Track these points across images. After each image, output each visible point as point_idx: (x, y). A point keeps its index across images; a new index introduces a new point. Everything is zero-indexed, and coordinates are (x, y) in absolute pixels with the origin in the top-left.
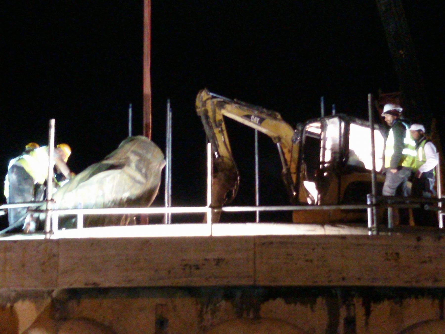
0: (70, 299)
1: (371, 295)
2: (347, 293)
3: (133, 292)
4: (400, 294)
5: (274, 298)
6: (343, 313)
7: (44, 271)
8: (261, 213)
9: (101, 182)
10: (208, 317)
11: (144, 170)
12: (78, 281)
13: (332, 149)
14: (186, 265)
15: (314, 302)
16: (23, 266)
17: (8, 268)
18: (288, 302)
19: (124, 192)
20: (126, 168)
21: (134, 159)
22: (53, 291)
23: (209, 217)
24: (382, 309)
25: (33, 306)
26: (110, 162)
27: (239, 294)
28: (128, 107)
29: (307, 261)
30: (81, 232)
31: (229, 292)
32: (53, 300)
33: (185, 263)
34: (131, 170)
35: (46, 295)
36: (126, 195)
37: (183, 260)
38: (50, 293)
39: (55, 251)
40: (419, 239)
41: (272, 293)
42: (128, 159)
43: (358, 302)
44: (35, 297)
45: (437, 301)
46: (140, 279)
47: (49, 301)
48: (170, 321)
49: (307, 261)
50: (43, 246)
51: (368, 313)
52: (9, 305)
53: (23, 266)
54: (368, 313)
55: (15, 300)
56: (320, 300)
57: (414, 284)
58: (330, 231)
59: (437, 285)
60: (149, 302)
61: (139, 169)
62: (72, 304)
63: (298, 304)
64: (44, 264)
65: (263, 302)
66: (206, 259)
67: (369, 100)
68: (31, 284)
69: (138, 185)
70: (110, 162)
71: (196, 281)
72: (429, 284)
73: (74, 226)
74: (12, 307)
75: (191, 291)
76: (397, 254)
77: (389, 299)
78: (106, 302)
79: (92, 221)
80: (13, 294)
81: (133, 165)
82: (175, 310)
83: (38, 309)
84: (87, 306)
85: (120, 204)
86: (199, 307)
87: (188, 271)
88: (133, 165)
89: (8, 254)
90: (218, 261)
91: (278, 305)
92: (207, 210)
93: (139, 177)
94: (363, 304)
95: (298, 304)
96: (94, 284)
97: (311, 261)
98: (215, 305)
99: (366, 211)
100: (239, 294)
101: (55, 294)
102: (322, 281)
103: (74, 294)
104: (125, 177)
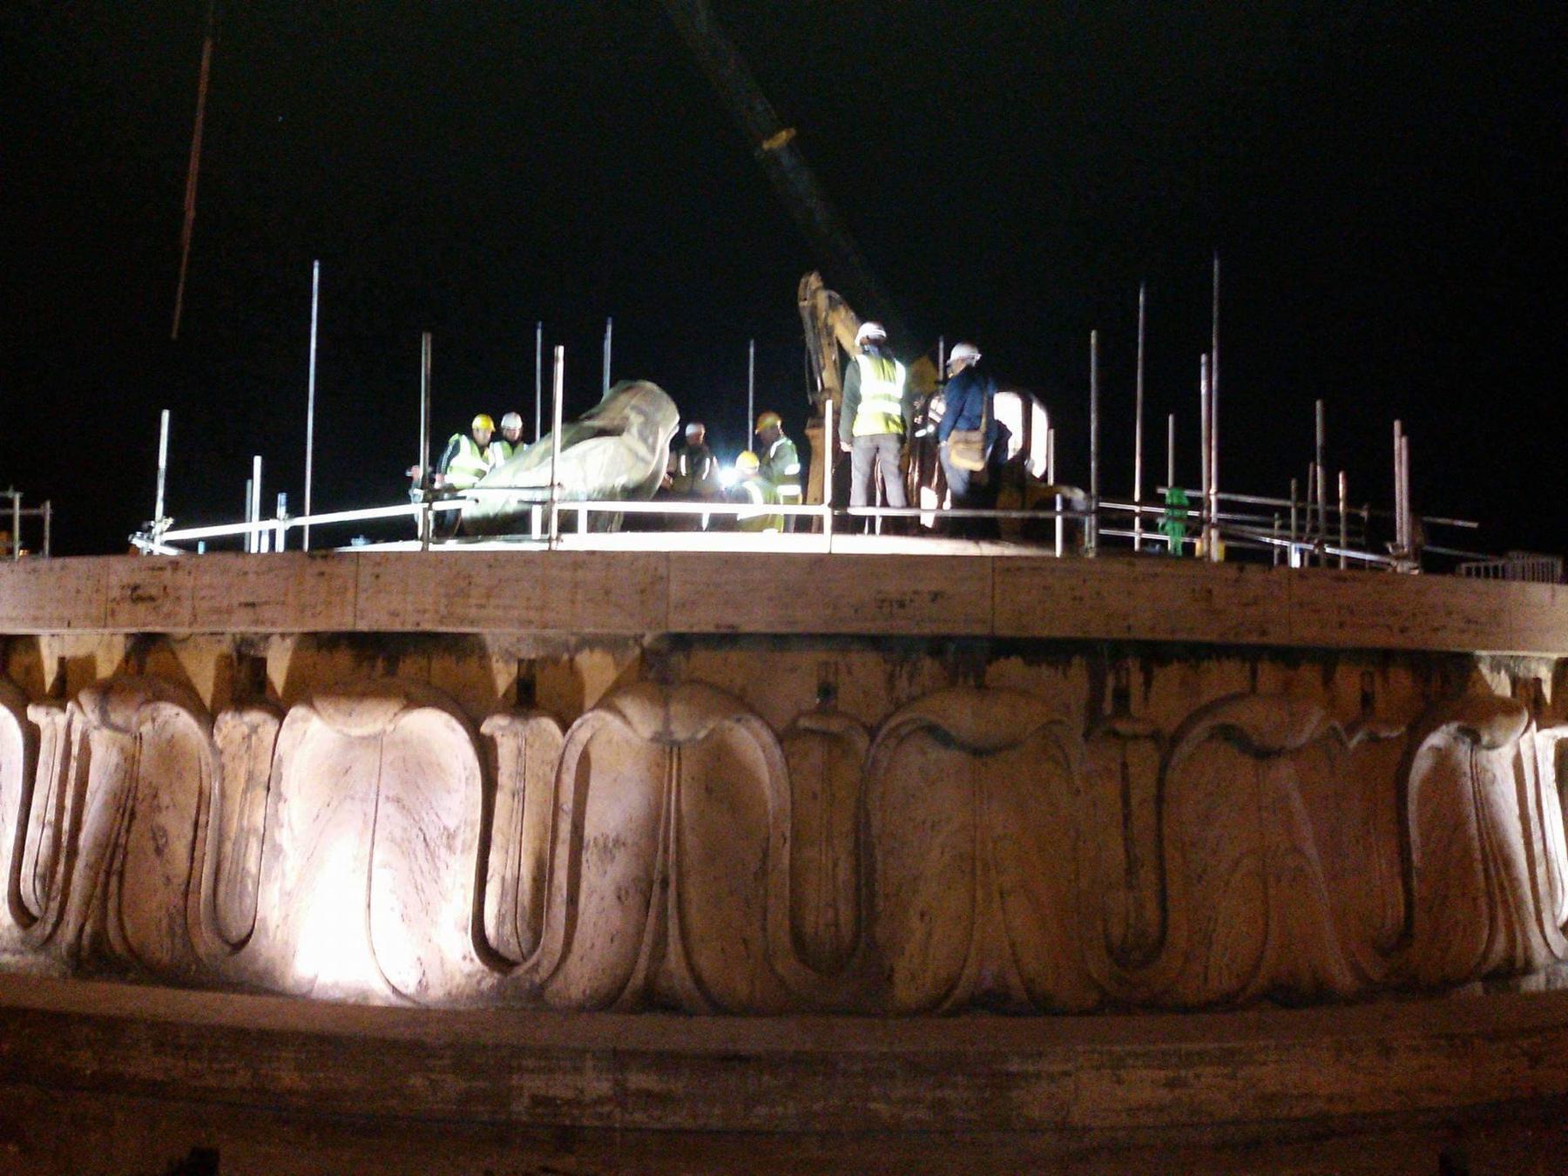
0: (671, 650)
1: (1154, 654)
2: (1119, 650)
3: (779, 641)
4: (1197, 653)
5: (1008, 657)
6: (1110, 681)
7: (642, 602)
8: (885, 519)
9: (583, 458)
10: (902, 684)
11: (650, 440)
12: (703, 620)
13: (418, 463)
14: (883, 601)
15: (1069, 663)
16: (607, 593)
17: (579, 597)
18: (1029, 662)
19: (618, 475)
20: (625, 436)
21: (636, 420)
22: (643, 636)
23: (828, 523)
24: (1169, 676)
25: (609, 659)
26: (597, 423)
27: (952, 647)
28: (535, 328)
29: (1075, 599)
30: (581, 541)
31: (937, 646)
32: (644, 652)
33: (880, 596)
34: (631, 439)
35: (631, 642)
36: (621, 481)
37: (880, 592)
38: (638, 639)
39: (662, 571)
40: (1241, 569)
41: (1003, 647)
42: (627, 418)
43: (1133, 665)
44: (612, 644)
45: (1248, 665)
46: (809, 619)
47: (637, 651)
48: (841, 690)
49: (1075, 599)
50: (641, 562)
51: (1148, 683)
52: (566, 657)
53: (607, 593)
54: (1148, 683)
55: (578, 648)
56: (1076, 660)
57: (1231, 638)
58: (987, 549)
59: (1265, 640)
60: (808, 660)
61: (643, 438)
62: (677, 659)
63: (1044, 667)
64: (643, 591)
65: (989, 662)
66: (915, 592)
67: (1093, 341)
68: (619, 624)
69: (641, 465)
70: (597, 423)
71: (903, 626)
72: (1254, 639)
73: (820, 529)
74: (572, 660)
75: (876, 642)
76: (1210, 592)
77: (1179, 661)
78: (735, 656)
79: (598, 522)
80: (573, 640)
81: (634, 430)
82: (850, 673)
83: (617, 664)
84: (703, 661)
85: (611, 496)
86: (889, 667)
87: (886, 610)
88: (634, 430)
89: (580, 573)
90: (936, 596)
91: (1013, 667)
92: (825, 512)
93: (642, 450)
94: (1142, 669)
95: (1044, 667)
96: (732, 627)
97: (1081, 599)
98: (915, 664)
99: (1054, 521)
100: (952, 647)
101: (647, 640)
102: (1096, 631)
103: (682, 642)
104: (622, 449)
